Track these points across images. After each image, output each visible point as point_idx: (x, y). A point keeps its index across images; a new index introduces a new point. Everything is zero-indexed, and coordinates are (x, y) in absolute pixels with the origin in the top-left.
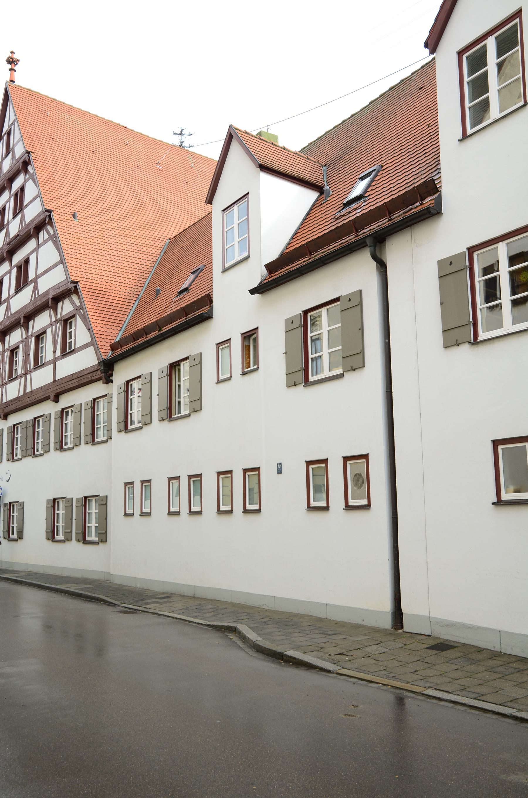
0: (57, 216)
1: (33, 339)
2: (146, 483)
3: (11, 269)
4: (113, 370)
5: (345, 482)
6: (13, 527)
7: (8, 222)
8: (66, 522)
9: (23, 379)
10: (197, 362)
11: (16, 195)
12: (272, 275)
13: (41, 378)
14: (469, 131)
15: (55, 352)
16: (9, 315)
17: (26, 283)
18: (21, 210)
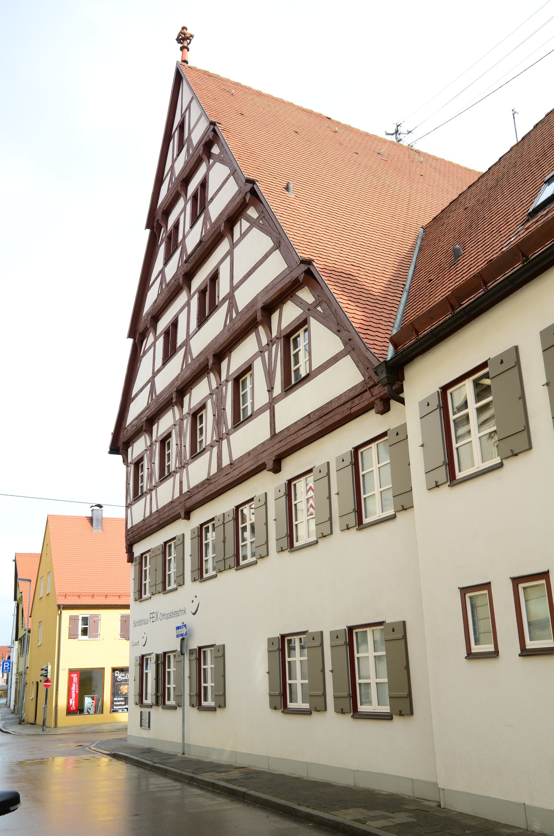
1: (158, 444)
3: (190, 298)
4: (403, 379)
6: (205, 688)
8: (214, 680)
13: (250, 438)
16: (190, 361)
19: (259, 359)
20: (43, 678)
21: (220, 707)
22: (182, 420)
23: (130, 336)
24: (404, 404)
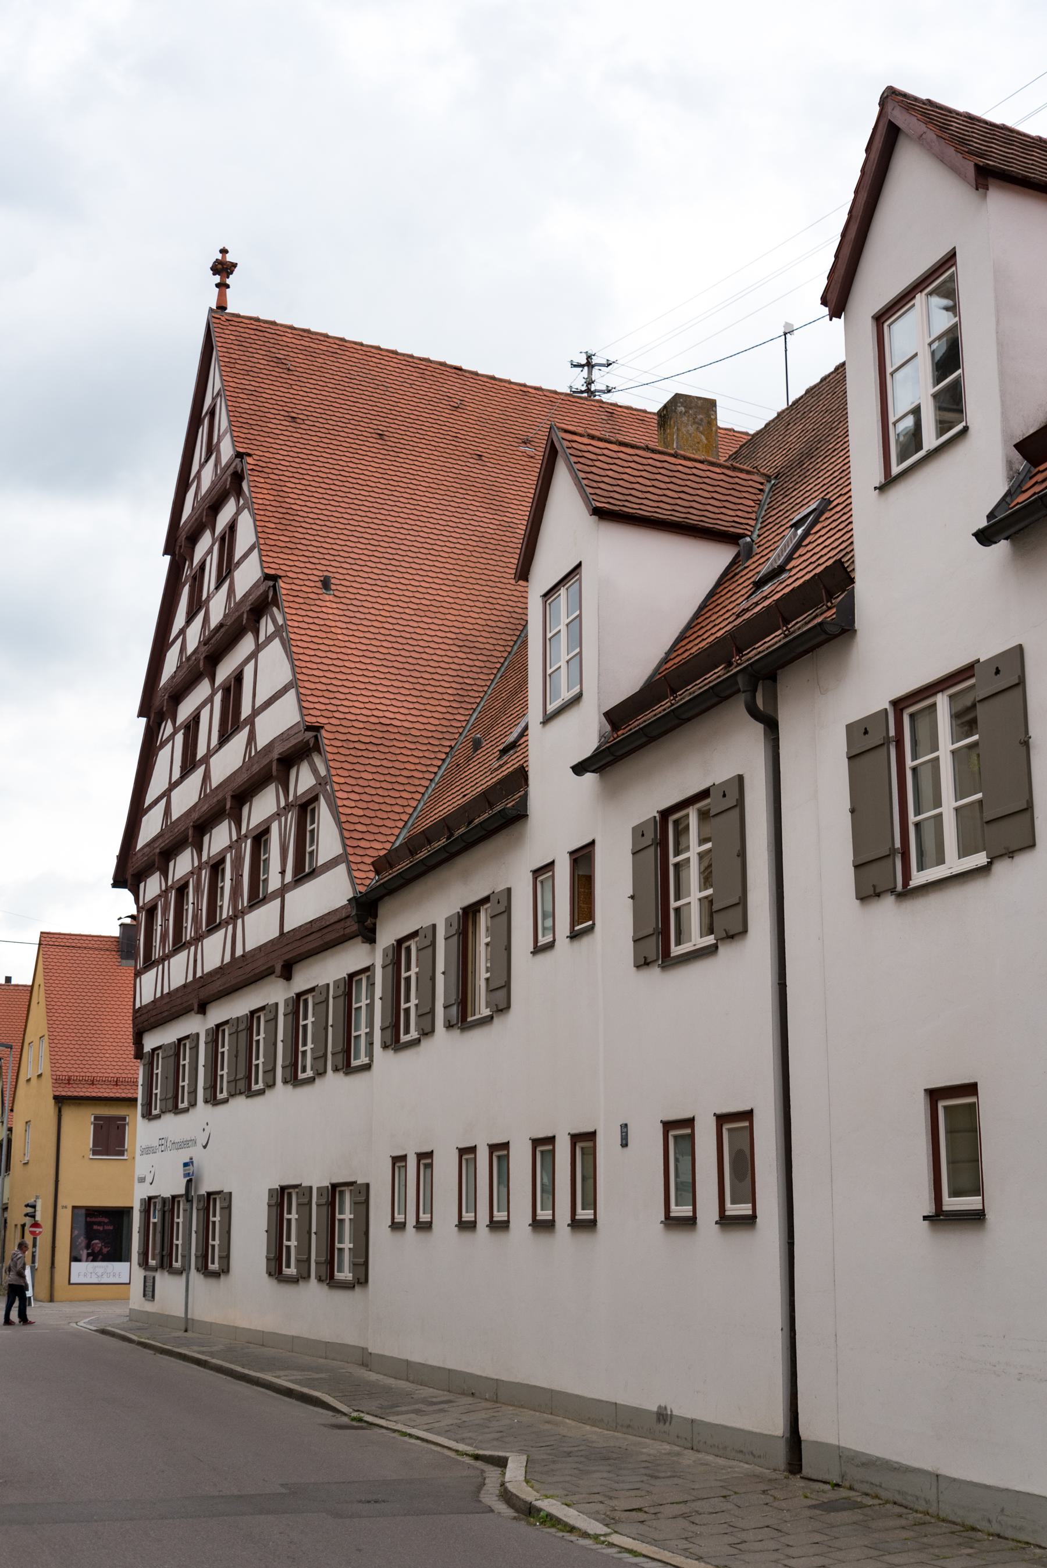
0: (288, 587)
2: (425, 1157)
4: (375, 916)
5: (728, 1167)
7: (208, 596)
8: (354, 1239)
9: (230, 927)
10: (501, 904)
11: (222, 539)
12: (620, 733)
13: (260, 928)
14: (895, 470)
15: (283, 872)
17: (237, 728)
18: (230, 572)
19: (276, 823)
20: (28, 1221)
21: (359, 1283)
22: (200, 868)
23: (141, 714)
24: (592, 843)
